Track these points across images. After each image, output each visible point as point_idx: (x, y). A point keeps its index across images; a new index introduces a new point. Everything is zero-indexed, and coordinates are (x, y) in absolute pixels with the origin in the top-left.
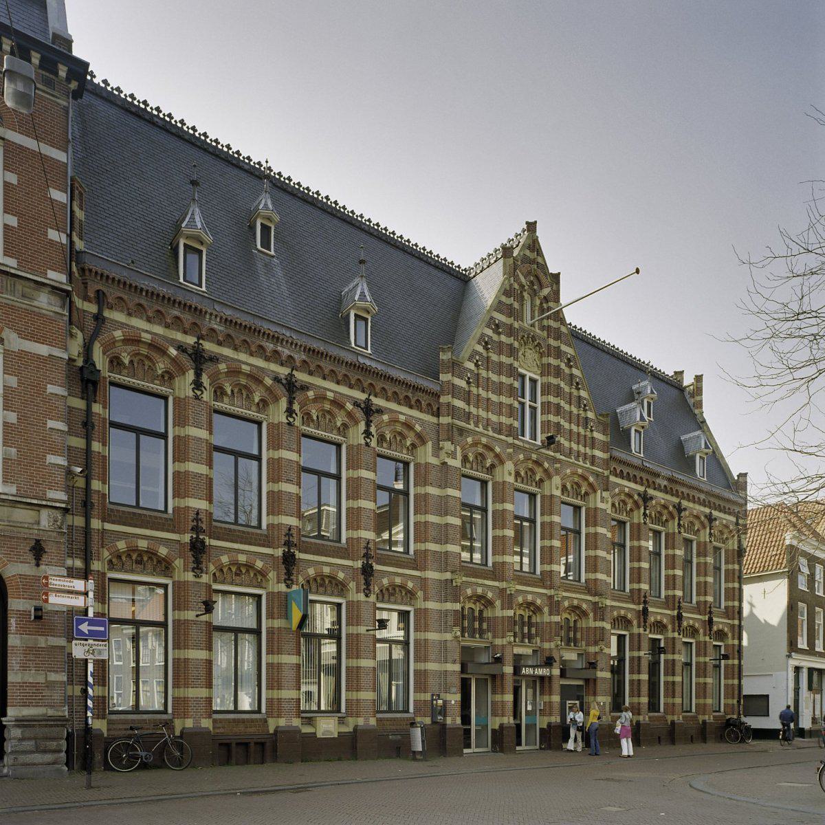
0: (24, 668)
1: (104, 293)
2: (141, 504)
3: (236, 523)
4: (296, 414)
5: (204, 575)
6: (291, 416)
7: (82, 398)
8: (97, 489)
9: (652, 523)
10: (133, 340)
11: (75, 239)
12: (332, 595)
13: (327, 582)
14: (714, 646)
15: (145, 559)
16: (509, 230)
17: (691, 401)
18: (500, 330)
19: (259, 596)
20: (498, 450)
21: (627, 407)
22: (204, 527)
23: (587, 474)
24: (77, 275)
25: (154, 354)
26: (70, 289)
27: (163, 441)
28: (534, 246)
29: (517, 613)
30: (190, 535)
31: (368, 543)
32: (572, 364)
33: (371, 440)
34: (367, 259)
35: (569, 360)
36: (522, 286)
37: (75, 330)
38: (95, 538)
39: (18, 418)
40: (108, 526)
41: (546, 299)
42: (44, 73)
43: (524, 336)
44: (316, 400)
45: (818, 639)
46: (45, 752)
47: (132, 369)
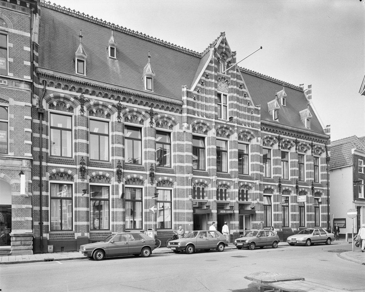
0: (17, 216)
1: (45, 81)
2: (63, 155)
3: (61, 156)
4: (154, 123)
5: (85, 180)
6: (120, 119)
7: (39, 119)
8: (44, 151)
9: (315, 154)
10: (57, 97)
11: (35, 63)
12: (139, 185)
13: (136, 180)
14: (315, 199)
15: (64, 175)
16: (212, 37)
17: (307, 96)
18: (209, 77)
19: (142, 189)
20: (208, 124)
21: (272, 102)
22: (85, 162)
23: (250, 131)
24: (36, 76)
25: (104, 108)
26: (32, 81)
27: (140, 142)
28: (224, 42)
29: (220, 189)
30: (80, 166)
31: (152, 165)
32: (242, 87)
33: (84, 113)
34: (151, 56)
35: (241, 86)
36: (218, 58)
37: (35, 96)
38: (44, 169)
39: (14, 129)
40: (49, 164)
41: (230, 62)
42: (22, 7)
43: (220, 78)
44: (130, 112)
45: (360, 192)
46: (24, 245)
47: (58, 108)
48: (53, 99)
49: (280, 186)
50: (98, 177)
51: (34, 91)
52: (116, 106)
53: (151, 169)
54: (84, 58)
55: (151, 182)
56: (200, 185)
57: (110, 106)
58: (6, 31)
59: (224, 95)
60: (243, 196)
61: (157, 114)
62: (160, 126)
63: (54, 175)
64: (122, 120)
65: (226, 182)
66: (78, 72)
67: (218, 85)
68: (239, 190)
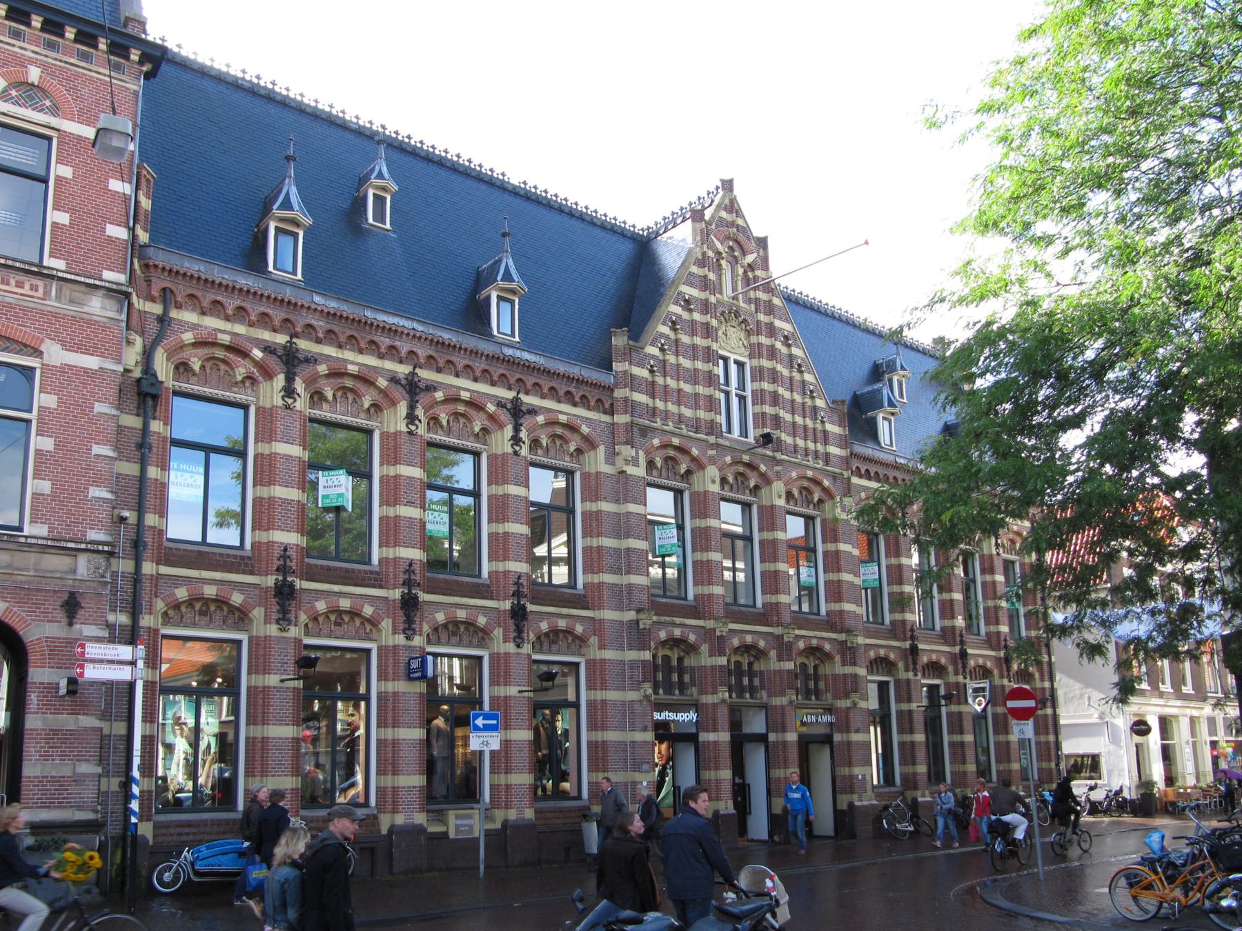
2: (209, 540)
5: (292, 628)
7: (138, 415)
15: (212, 608)
23: (820, 477)
24: (138, 272)
28: (732, 206)
31: (519, 578)
38: (146, 587)
48: (322, 382)
49: (519, 614)
50: (333, 617)
51: (134, 322)
52: (404, 382)
53: (518, 594)
54: (298, 224)
55: (514, 638)
56: (671, 649)
57: (382, 383)
58: (53, 128)
59: (736, 362)
60: (667, 677)
61: (533, 411)
62: (325, 406)
63: (177, 606)
64: (422, 429)
65: (570, 621)
66: (275, 268)
67: (720, 333)
68: (654, 656)
